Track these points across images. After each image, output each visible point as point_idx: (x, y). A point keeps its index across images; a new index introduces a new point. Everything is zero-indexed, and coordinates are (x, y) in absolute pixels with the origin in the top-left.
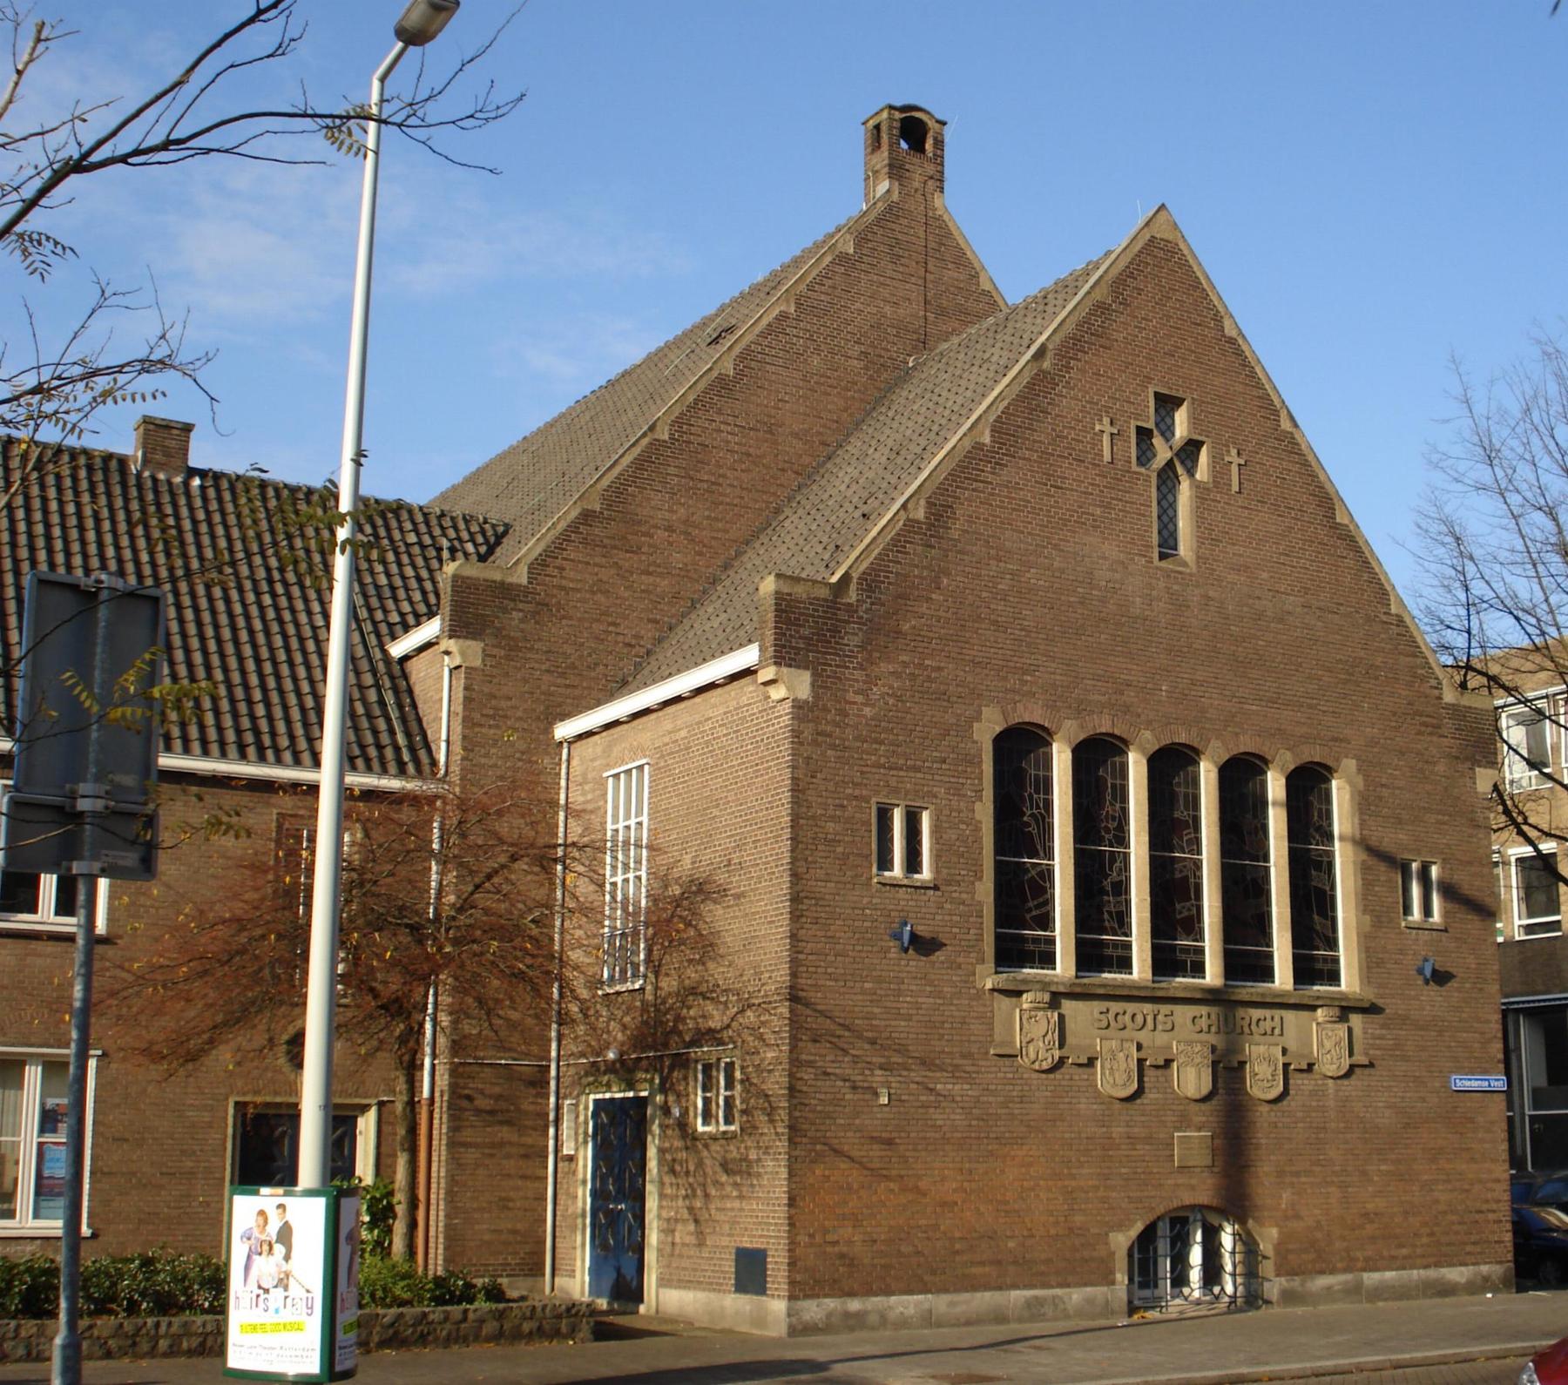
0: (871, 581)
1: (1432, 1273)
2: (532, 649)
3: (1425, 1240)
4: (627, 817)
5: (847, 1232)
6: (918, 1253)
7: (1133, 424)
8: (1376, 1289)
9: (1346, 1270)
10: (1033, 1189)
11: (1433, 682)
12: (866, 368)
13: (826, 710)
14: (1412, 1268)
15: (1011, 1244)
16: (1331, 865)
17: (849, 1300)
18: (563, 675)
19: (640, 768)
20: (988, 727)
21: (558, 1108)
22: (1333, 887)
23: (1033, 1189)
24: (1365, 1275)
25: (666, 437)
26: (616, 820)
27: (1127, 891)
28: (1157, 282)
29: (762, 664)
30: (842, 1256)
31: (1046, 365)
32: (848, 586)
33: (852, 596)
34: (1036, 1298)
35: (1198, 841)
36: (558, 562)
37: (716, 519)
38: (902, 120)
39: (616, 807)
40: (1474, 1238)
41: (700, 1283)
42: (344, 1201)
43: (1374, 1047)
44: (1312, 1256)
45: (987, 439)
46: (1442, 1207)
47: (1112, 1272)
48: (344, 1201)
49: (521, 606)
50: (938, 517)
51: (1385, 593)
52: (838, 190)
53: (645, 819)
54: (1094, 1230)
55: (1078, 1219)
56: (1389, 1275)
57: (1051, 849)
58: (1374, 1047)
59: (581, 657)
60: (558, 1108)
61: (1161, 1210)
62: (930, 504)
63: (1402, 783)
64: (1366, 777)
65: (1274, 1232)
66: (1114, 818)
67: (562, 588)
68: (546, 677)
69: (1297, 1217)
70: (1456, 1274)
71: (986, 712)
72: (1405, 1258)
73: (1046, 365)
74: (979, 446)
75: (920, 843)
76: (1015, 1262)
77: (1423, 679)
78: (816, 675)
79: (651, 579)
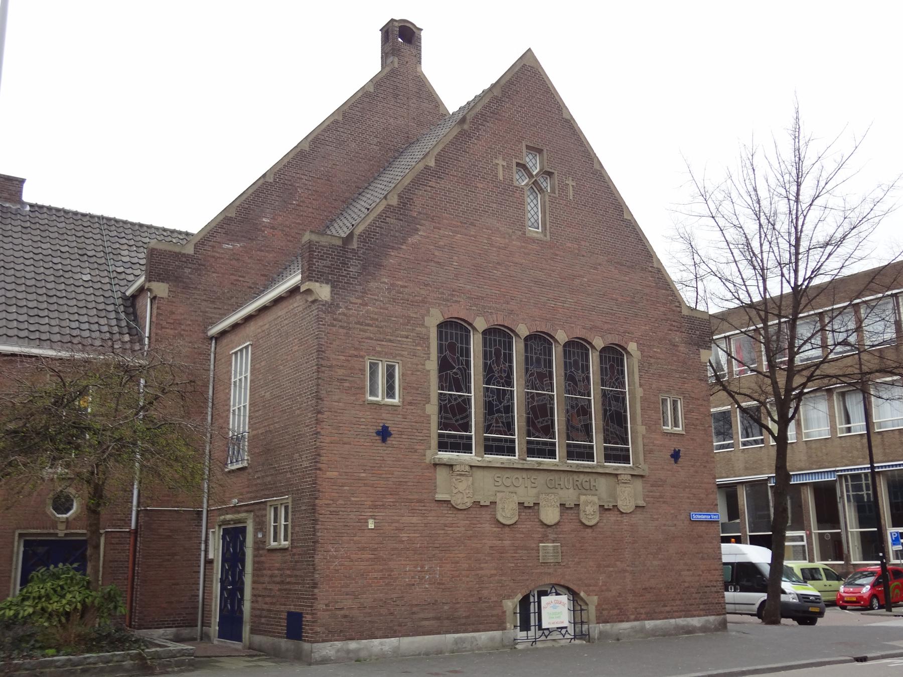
0: (366, 237)
1: (681, 621)
2: (196, 288)
3: (678, 602)
4: (241, 374)
5: (348, 602)
6: (391, 614)
7: (514, 161)
8: (652, 630)
9: (636, 619)
10: (458, 576)
11: (677, 304)
12: (380, 150)
13: (338, 306)
14: (671, 618)
15: (446, 607)
16: (624, 399)
17: (349, 642)
18: (213, 302)
19: (247, 347)
20: (434, 318)
21: (207, 534)
22: (625, 411)
23: (458, 576)
24: (647, 622)
25: (272, 181)
26: (235, 377)
27: (513, 412)
28: (525, 91)
29: (303, 281)
30: (345, 616)
31: (466, 127)
32: (352, 238)
33: (355, 245)
34: (461, 638)
35: (552, 384)
36: (210, 243)
37: (299, 224)
38: (400, 27)
39: (236, 371)
40: (705, 601)
41: (260, 631)
42: (543, 598)
43: (648, 496)
44: (615, 612)
45: (432, 163)
46: (686, 585)
47: (504, 623)
48: (543, 598)
49: (190, 265)
50: (405, 204)
51: (651, 257)
52: (366, 64)
53: (249, 374)
54: (495, 599)
55: (485, 593)
56: (658, 622)
57: (470, 388)
58: (648, 496)
59: (224, 293)
60: (207, 534)
61: (532, 586)
62: (400, 197)
63: (662, 356)
64: (642, 352)
65: (596, 598)
66: (505, 371)
67: (213, 257)
68: (204, 303)
69: (609, 590)
70: (696, 622)
71: (432, 311)
72: (668, 612)
73: (466, 127)
74: (427, 168)
75: (394, 382)
76: (447, 618)
77: (672, 302)
78: (333, 287)
79: (263, 254)
